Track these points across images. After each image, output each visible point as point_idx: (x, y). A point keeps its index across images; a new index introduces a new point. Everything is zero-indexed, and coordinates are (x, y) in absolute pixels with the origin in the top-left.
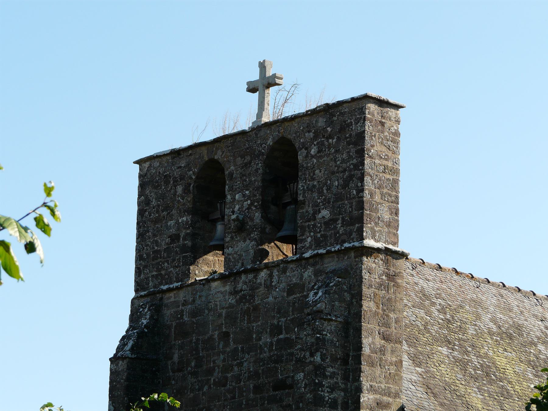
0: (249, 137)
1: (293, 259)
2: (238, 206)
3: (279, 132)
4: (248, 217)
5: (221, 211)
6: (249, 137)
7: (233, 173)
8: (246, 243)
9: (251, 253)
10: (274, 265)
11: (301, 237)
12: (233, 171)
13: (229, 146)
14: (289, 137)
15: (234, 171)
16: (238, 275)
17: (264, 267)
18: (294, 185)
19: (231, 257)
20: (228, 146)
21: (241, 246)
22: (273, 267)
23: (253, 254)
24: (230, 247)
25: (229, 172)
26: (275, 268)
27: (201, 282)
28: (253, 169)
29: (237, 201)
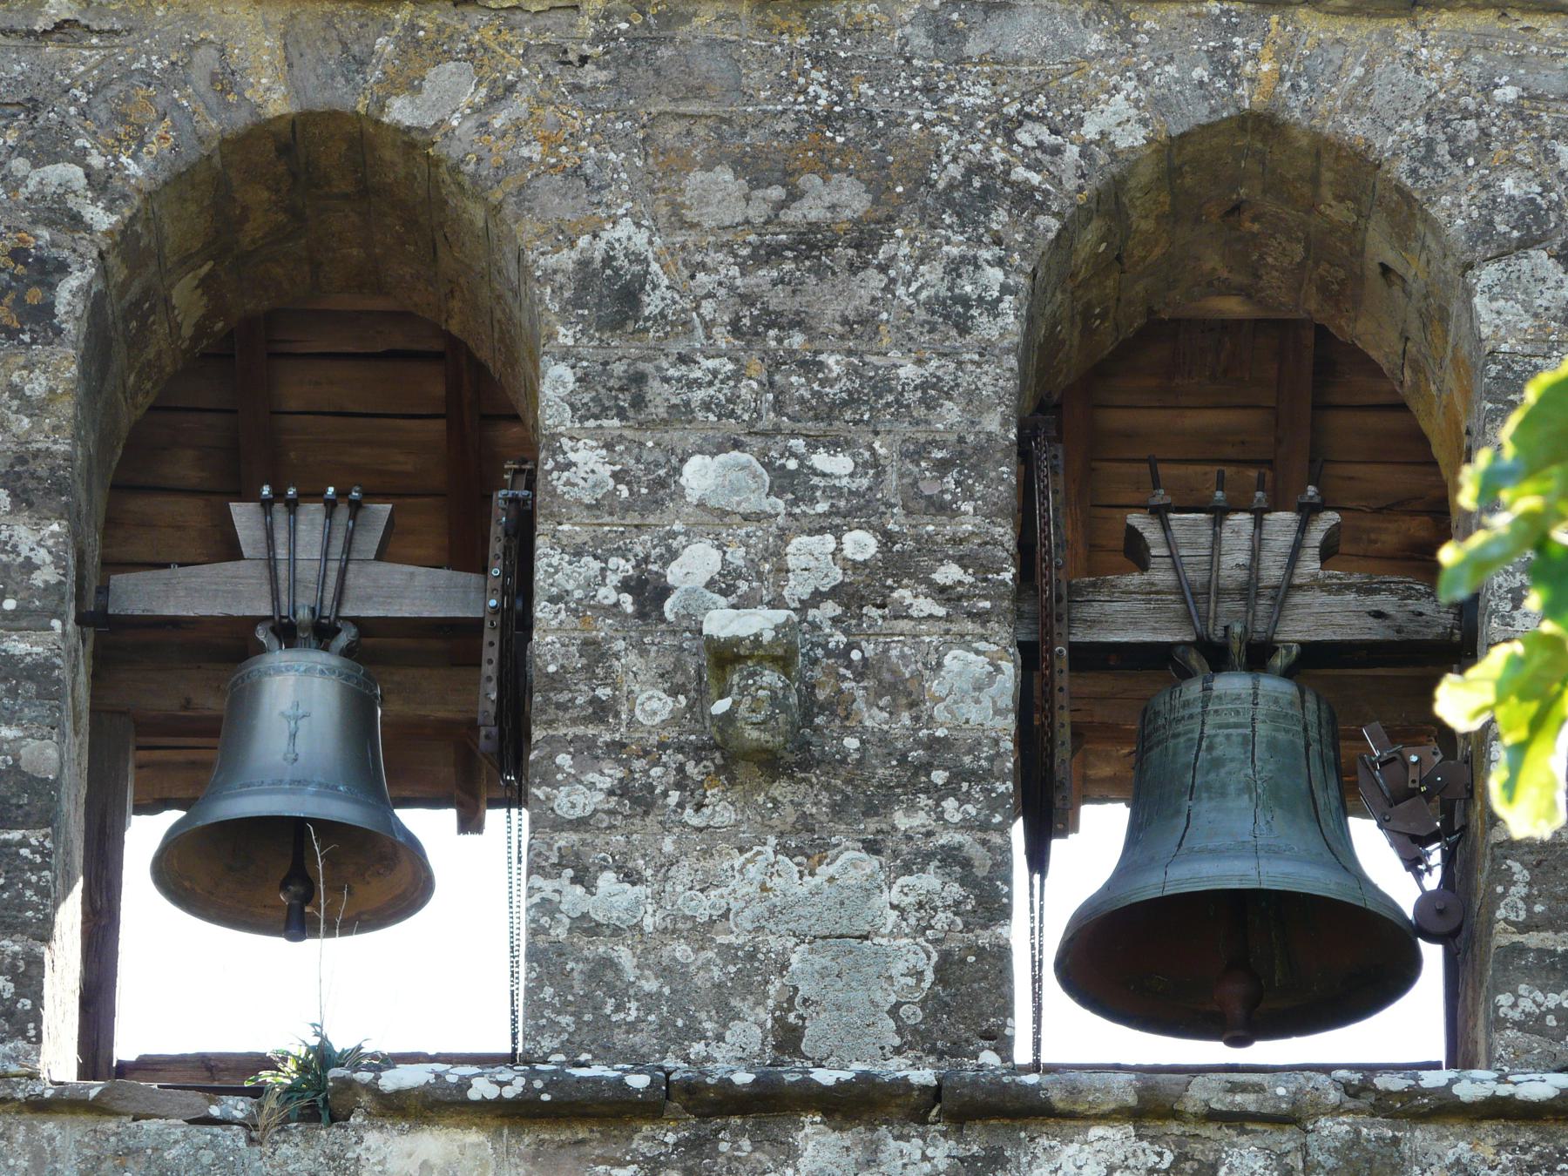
0: (844, 32)
1: (1512, 1096)
2: (716, 555)
3: (1221, 62)
4: (850, 665)
5: (283, 571)
6: (844, 32)
7: (642, 279)
8: (824, 871)
9: (899, 967)
10: (1252, 1108)
11: (1550, 934)
12: (637, 258)
13: (584, 60)
14: (1356, 129)
15: (655, 267)
16: (736, 1121)
17: (1132, 1100)
18: (1303, 528)
19: (625, 956)
20: (572, 57)
21: (764, 888)
22: (1236, 1120)
23: (929, 977)
24: (603, 868)
25: (584, 264)
26: (1243, 1132)
27: (212, 1102)
28: (901, 291)
29: (701, 505)
